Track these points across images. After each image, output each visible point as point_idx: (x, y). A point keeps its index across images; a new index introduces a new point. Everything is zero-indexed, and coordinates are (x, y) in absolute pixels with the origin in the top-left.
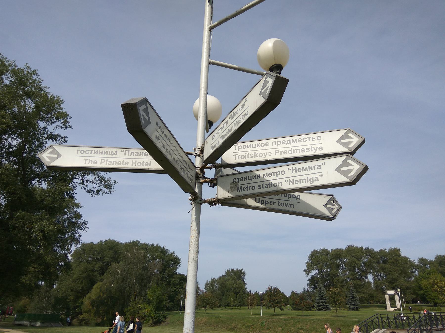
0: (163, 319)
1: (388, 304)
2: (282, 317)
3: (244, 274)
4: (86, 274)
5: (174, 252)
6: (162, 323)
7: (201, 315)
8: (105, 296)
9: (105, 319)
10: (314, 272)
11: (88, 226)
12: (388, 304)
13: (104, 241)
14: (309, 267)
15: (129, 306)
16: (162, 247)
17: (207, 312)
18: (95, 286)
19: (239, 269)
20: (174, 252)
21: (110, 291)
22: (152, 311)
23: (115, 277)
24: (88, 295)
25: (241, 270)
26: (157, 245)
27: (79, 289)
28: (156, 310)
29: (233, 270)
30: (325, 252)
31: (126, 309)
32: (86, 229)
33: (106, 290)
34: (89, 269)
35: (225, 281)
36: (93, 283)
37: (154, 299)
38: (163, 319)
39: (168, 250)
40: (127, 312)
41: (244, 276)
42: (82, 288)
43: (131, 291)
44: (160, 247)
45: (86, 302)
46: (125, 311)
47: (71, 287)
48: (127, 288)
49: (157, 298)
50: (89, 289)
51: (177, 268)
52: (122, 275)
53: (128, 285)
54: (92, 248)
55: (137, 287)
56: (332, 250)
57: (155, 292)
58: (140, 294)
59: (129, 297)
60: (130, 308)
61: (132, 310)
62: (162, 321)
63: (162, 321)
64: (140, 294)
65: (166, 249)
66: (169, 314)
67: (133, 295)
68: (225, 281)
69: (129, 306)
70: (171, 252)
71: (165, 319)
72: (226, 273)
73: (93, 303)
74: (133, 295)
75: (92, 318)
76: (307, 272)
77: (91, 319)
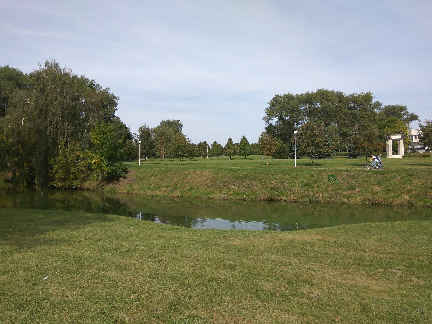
0: (123, 174)
1: (390, 150)
2: (321, 168)
3: (181, 125)
6: (121, 179)
7: (194, 166)
8: (10, 140)
9: (17, 174)
10: (274, 121)
12: (390, 150)
14: (270, 113)
15: (58, 155)
16: (90, 80)
17: (233, 161)
21: (19, 133)
23: (24, 112)
25: (178, 121)
26: (82, 77)
28: (109, 161)
29: (168, 121)
30: (289, 97)
31: (52, 159)
33: (12, 131)
35: (165, 132)
37: (103, 144)
38: (123, 174)
39: (98, 85)
40: (56, 164)
41: (181, 127)
44: (87, 80)
46: (51, 163)
48: (50, 128)
49: (109, 141)
51: (115, 110)
53: (51, 122)
55: (67, 127)
56: (297, 95)
58: (73, 136)
59: (55, 143)
60: (61, 158)
61: (64, 161)
62: (121, 176)
63: (121, 176)
64: (73, 136)
65: (96, 84)
66: (130, 166)
68: (165, 132)
69: (58, 155)
71: (126, 173)
72: (161, 124)
74: (61, 139)
76: (266, 120)
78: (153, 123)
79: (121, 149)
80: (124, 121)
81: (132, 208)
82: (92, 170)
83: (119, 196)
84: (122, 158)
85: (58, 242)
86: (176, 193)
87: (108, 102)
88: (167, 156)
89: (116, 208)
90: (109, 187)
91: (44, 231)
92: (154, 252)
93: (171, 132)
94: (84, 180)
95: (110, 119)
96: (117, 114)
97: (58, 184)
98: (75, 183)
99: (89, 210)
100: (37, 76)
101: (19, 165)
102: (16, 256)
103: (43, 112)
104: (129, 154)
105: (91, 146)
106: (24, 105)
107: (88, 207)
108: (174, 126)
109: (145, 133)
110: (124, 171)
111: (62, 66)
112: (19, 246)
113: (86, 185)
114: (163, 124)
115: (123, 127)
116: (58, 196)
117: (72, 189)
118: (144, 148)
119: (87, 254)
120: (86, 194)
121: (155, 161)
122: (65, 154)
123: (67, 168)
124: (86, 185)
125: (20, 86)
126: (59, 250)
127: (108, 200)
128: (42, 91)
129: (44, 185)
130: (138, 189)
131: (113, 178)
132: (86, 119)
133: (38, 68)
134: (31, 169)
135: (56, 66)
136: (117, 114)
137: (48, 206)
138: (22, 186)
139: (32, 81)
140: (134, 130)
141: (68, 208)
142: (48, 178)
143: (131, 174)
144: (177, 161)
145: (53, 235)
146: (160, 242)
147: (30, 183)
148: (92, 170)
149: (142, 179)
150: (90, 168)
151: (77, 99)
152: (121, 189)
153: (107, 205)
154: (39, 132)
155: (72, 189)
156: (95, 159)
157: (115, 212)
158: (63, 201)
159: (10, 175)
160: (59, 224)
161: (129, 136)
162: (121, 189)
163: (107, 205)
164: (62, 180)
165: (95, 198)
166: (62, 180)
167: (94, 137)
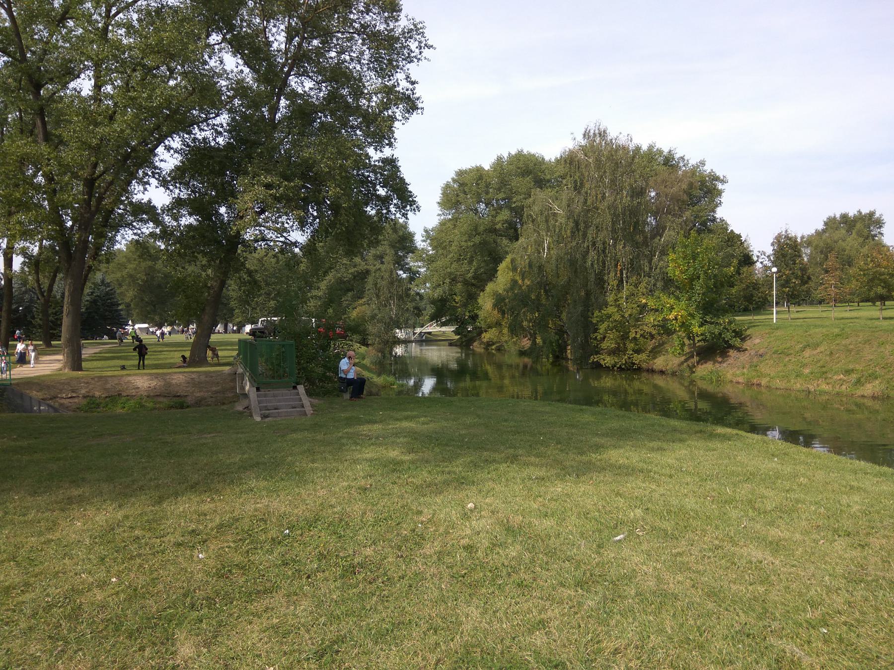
0: (737, 342)
4: (477, 239)
5: (703, 163)
6: (732, 353)
11: (431, 35)
13: (506, 156)
15: (606, 304)
18: (502, 266)
19: (865, 211)
20: (703, 163)
22: (692, 316)
24: (490, 287)
25: (872, 214)
26: (651, 147)
27: (470, 275)
31: (597, 313)
32: (426, 52)
33: (530, 265)
34: (481, 229)
35: (836, 242)
36: (497, 259)
37: (693, 279)
38: (737, 342)
39: (682, 158)
41: (880, 227)
42: (475, 273)
43: (604, 263)
44: (660, 152)
45: (486, 303)
47: (450, 273)
48: (592, 254)
50: (491, 275)
52: (570, 215)
53: (594, 244)
54: (480, 178)
55: (623, 251)
57: (694, 257)
58: (634, 268)
59: (601, 282)
60: (611, 310)
62: (731, 347)
63: (731, 347)
64: (634, 268)
65: (677, 156)
67: (612, 274)
69: (606, 304)
70: (693, 162)
71: (743, 340)
73: (499, 302)
74: (612, 274)
75: (506, 338)
77: (506, 342)
78: (805, 224)
79: (730, 288)
80: (735, 226)
81: (759, 417)
82: (669, 332)
83: (728, 390)
84: (732, 308)
85: (627, 471)
86: (869, 389)
87: (704, 189)
88: (840, 300)
89: (719, 412)
90: (704, 369)
91: (597, 448)
92: (847, 524)
93: (851, 242)
94: (655, 352)
95: (707, 226)
96: (720, 213)
97: (608, 360)
98: (638, 358)
99: (666, 413)
100: (569, 160)
101: (541, 325)
102: (559, 488)
103: (579, 225)
104: (749, 298)
105: (668, 283)
106: (549, 216)
107: (663, 406)
108: (865, 226)
109: (787, 249)
110: (738, 334)
111: (612, 134)
112: (564, 472)
113: (659, 363)
114: (831, 223)
115: (734, 239)
116: (607, 382)
117: (632, 370)
118: (784, 283)
119: (690, 503)
120: (659, 381)
121: (810, 312)
122: (619, 302)
123: (622, 329)
124: (659, 363)
125: (540, 183)
126: (635, 486)
127: (704, 395)
128: (578, 187)
129: (582, 361)
130: (771, 375)
131: (714, 349)
132: (658, 231)
133: (570, 145)
134: (561, 332)
135: (603, 134)
136: (720, 213)
137: (590, 399)
138: (546, 362)
139: (561, 170)
140: (761, 246)
141: (625, 405)
142: (588, 349)
143: (756, 342)
144: (869, 311)
145: (618, 455)
146: (856, 503)
147: (559, 357)
148: (669, 332)
149: (778, 352)
150: (665, 329)
151: (640, 193)
152: (731, 374)
153: (703, 405)
154: (572, 263)
155: (632, 370)
156: (677, 310)
157: (720, 421)
158: (614, 393)
159: (526, 343)
160: (623, 435)
161: (747, 260)
162: (731, 374)
163: (703, 405)
164: (613, 352)
165: (677, 390)
166: (613, 352)
167: (674, 266)
